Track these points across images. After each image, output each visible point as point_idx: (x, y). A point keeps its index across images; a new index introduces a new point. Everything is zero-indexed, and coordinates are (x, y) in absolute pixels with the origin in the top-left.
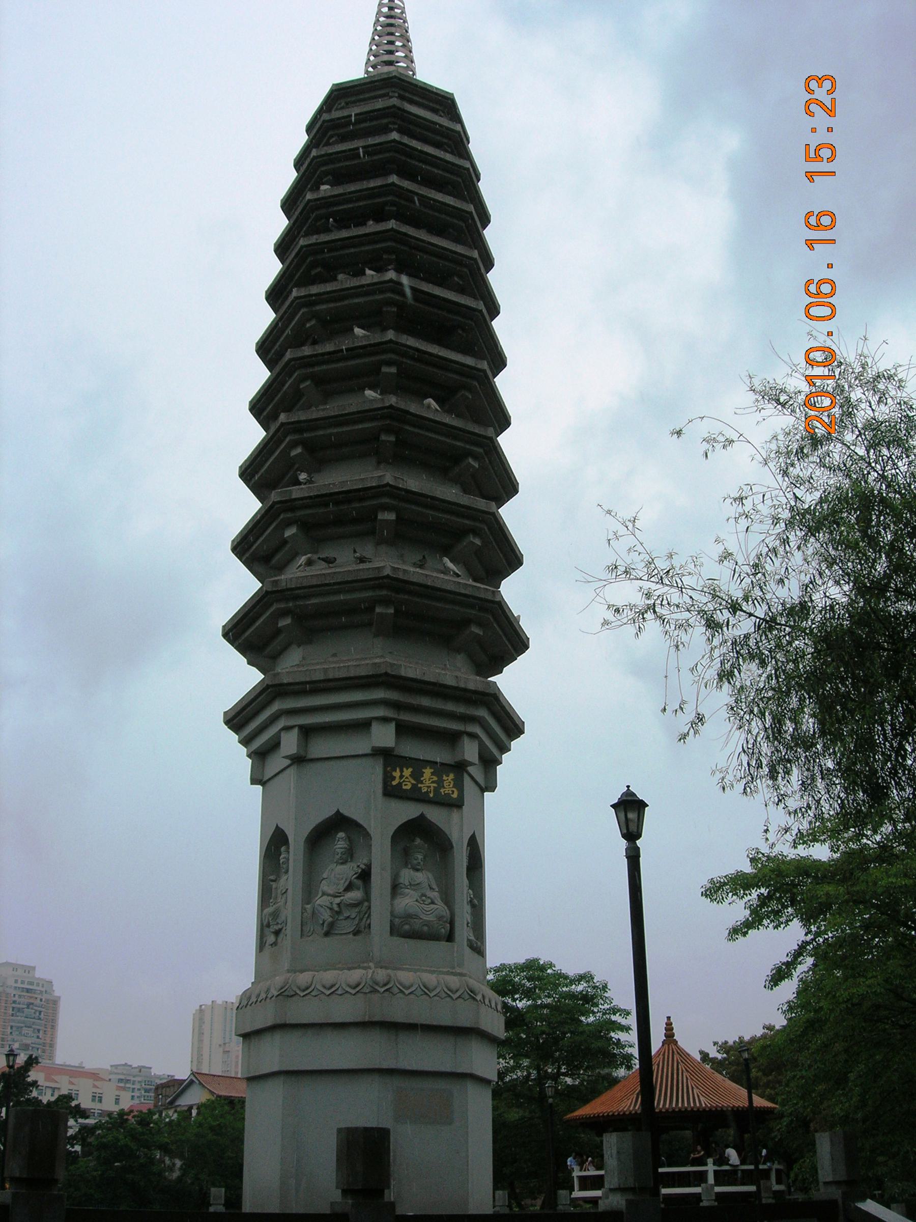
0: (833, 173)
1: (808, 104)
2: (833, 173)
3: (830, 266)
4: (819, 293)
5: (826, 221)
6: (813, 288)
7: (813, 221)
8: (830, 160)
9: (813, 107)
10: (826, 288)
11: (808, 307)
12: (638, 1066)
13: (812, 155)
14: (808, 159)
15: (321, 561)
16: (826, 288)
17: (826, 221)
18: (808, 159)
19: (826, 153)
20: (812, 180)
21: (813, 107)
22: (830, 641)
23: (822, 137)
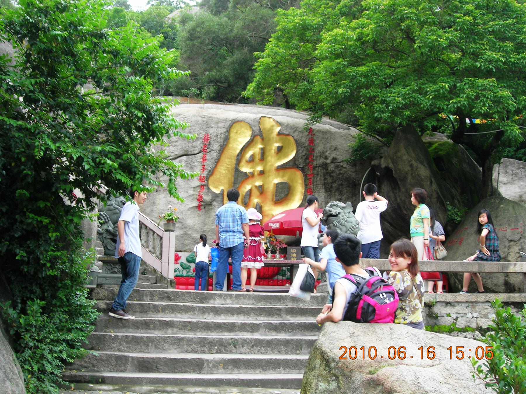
0: (451, 358)
1: (345, 347)
2: (451, 358)
3: (412, 357)
4: (400, 352)
5: (431, 355)
6: (402, 350)
7: (431, 350)
8: (457, 357)
9: (343, 350)
10: (402, 355)
11: (394, 348)
12: (60, 194)
13: (460, 349)
14: (458, 348)
15: (434, 230)
16: (402, 355)
17: (431, 355)
18: (458, 348)
19: (460, 355)
20: (419, 349)
21: (343, 350)
22: (237, 368)
23: (467, 354)
